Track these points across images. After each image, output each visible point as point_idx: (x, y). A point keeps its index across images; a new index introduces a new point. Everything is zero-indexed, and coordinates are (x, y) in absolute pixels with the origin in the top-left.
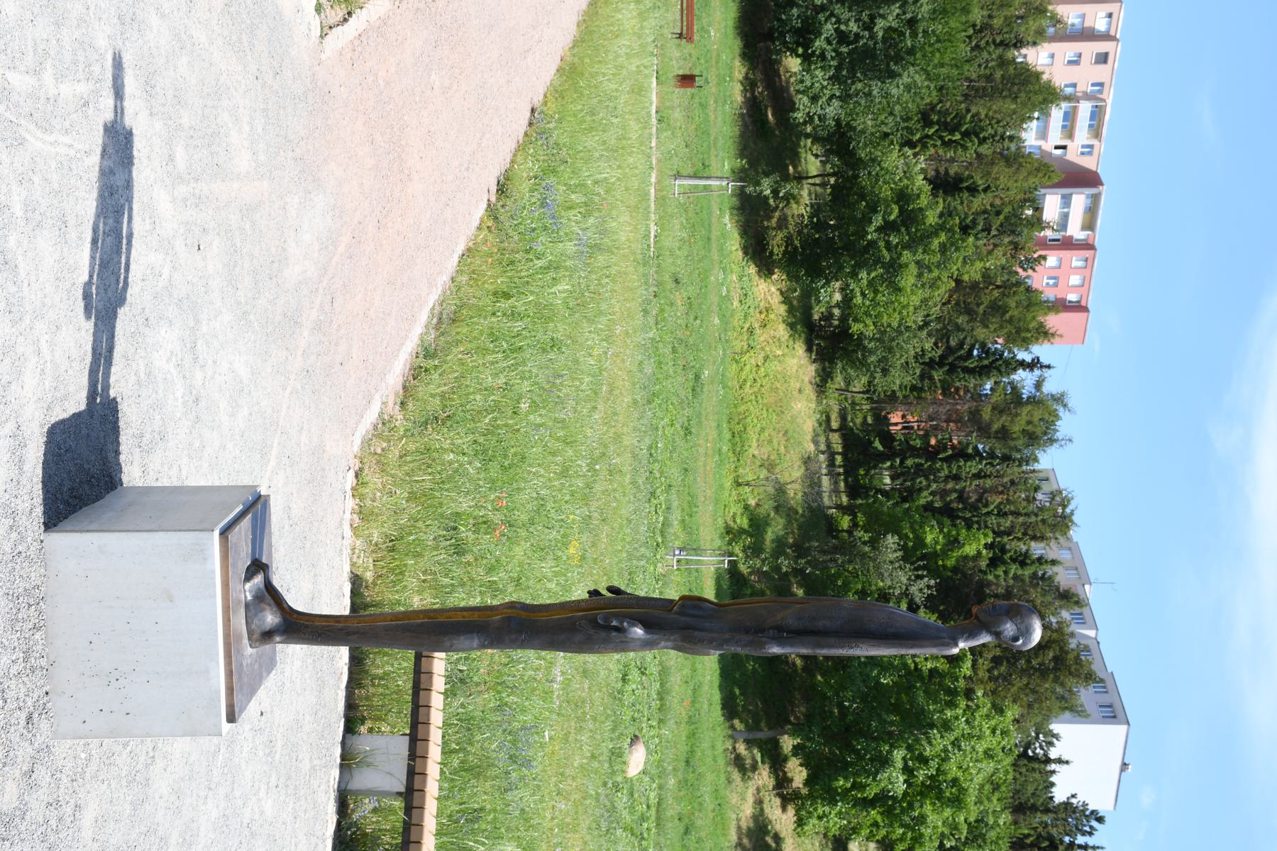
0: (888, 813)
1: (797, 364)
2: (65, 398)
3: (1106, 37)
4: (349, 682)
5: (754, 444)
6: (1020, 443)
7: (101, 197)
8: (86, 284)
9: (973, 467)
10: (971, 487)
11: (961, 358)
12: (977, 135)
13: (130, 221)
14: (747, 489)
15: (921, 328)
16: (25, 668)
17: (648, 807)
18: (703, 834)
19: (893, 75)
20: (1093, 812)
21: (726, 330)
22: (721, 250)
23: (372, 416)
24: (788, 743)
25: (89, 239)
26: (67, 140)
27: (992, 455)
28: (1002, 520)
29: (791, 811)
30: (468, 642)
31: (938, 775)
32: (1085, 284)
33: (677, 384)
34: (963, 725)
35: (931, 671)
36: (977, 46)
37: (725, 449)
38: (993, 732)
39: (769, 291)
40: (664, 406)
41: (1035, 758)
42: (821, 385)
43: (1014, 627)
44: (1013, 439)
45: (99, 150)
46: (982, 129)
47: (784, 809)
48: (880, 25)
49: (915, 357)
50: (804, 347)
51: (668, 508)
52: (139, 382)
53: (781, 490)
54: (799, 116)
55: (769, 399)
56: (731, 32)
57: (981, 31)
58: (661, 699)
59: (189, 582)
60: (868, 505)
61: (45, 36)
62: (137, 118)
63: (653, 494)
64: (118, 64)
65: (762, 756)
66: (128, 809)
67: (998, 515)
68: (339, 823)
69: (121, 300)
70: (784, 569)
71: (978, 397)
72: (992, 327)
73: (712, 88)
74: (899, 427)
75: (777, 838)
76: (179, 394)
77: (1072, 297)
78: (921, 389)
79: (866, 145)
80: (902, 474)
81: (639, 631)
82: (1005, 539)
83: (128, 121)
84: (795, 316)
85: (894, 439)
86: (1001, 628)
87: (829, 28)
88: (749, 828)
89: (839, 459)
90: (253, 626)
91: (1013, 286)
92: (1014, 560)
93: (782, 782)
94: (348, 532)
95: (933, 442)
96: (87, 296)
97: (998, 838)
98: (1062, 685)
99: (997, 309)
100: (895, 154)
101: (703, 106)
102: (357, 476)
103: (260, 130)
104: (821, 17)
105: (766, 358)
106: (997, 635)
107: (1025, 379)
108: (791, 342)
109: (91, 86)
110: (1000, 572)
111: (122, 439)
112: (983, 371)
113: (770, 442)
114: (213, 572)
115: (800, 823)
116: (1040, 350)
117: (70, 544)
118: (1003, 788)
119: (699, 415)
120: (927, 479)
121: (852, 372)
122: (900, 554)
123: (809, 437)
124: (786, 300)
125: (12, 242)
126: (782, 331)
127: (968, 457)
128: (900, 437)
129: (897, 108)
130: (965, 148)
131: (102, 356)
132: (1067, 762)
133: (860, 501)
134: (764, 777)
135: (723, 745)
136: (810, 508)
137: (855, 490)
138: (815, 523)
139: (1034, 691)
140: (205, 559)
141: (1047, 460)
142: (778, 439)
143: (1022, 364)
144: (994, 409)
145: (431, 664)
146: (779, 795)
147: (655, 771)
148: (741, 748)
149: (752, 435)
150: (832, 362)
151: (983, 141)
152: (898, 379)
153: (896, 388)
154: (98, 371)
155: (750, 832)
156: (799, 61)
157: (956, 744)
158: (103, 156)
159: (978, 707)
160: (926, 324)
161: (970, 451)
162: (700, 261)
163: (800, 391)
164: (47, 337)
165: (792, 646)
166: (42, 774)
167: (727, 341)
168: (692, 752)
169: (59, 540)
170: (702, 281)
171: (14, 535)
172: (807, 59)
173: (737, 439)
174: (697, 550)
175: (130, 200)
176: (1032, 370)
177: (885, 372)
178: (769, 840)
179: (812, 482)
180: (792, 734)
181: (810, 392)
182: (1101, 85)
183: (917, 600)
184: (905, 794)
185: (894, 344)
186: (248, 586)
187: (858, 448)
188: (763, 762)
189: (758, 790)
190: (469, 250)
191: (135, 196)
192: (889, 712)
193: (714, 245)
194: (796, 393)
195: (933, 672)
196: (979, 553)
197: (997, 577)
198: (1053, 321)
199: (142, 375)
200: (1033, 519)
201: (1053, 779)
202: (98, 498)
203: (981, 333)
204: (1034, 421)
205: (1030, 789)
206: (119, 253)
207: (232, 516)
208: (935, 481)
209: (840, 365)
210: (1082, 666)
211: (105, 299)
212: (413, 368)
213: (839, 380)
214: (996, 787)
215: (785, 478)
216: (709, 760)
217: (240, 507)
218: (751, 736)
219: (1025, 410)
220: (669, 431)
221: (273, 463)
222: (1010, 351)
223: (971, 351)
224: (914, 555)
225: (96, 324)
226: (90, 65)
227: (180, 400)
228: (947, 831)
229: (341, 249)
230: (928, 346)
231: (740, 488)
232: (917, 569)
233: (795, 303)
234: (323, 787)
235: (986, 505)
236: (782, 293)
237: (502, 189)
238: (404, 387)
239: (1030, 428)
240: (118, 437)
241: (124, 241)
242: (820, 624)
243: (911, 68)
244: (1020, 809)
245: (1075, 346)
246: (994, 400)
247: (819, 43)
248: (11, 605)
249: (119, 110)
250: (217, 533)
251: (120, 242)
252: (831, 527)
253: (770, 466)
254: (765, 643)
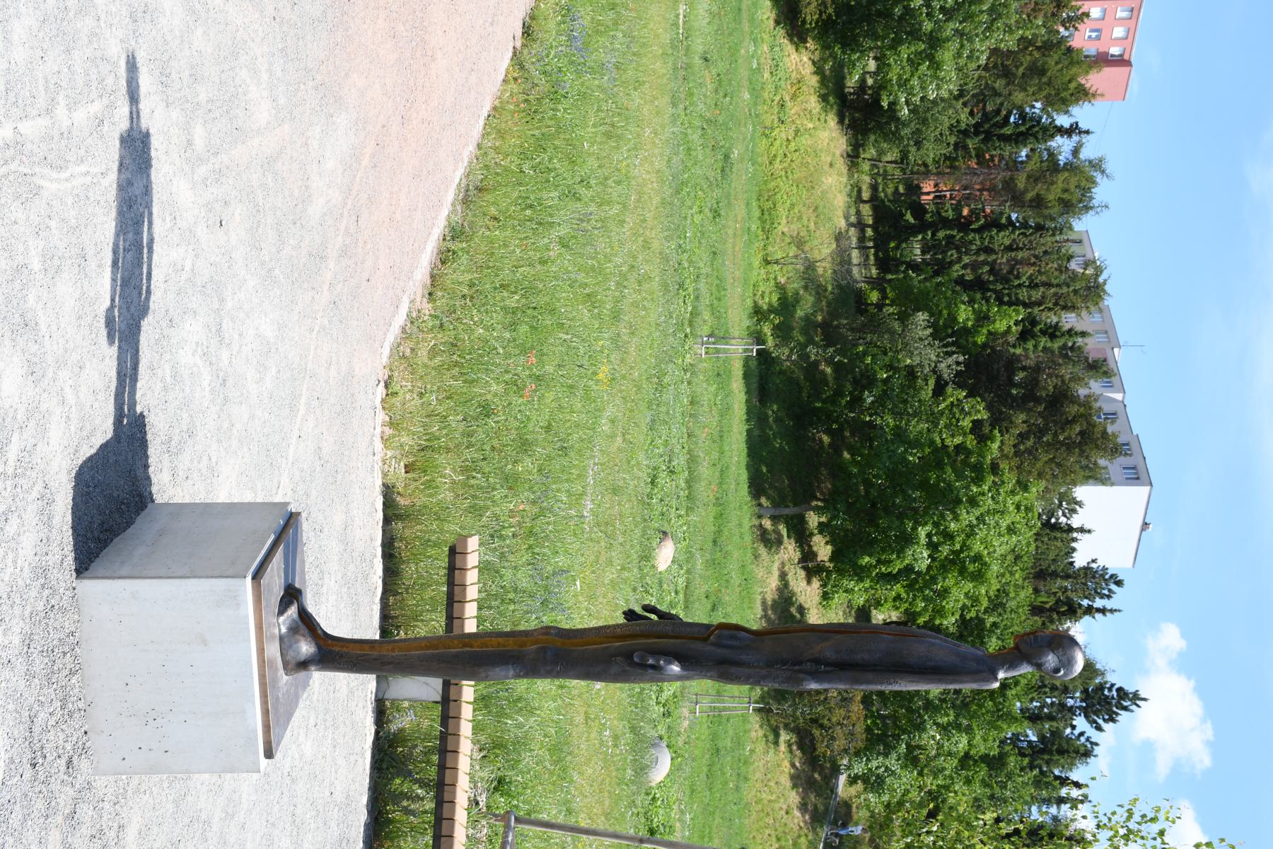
0: (910, 587)
1: (830, 137)
2: (92, 433)
4: (383, 594)
5: (784, 221)
6: (1054, 211)
7: (120, 213)
8: (108, 310)
9: (1004, 238)
10: (1003, 259)
11: (997, 125)
13: (150, 223)
14: (776, 267)
15: (957, 98)
16: (63, 715)
17: (676, 592)
18: (729, 609)
20: (1112, 576)
21: (756, 104)
22: (752, 20)
23: (400, 319)
24: (813, 520)
25: (109, 263)
26: (83, 168)
27: (1025, 225)
28: (1033, 293)
29: (816, 583)
30: (503, 673)
31: (961, 551)
32: (1130, 36)
33: (706, 165)
34: (990, 501)
35: (957, 447)
37: (754, 227)
38: (1018, 507)
39: (799, 62)
41: (1057, 527)
42: (853, 158)
43: (1056, 659)
44: (1047, 208)
45: (115, 166)
47: (809, 582)
50: (836, 119)
51: (697, 298)
52: (165, 389)
53: (810, 266)
58: (689, 487)
59: (222, 621)
60: (898, 279)
61: (56, 69)
62: (154, 118)
63: (681, 285)
64: (132, 66)
65: (788, 531)
66: (170, 807)
67: (1029, 286)
68: (377, 733)
69: (144, 311)
70: (813, 357)
71: (1015, 165)
72: (1031, 90)
74: (931, 197)
75: (801, 609)
76: (205, 383)
77: (1115, 51)
78: (956, 159)
80: (934, 246)
81: (675, 668)
82: (1036, 310)
83: (144, 123)
84: (827, 87)
85: (926, 211)
86: (1043, 660)
88: (774, 600)
89: (869, 232)
90: (288, 658)
91: (1052, 45)
92: (1043, 332)
93: (808, 556)
94: (378, 445)
95: (965, 212)
96: (109, 322)
97: (1018, 607)
98: (1087, 457)
99: (1037, 70)
102: (386, 387)
103: (279, 74)
105: (797, 132)
106: (1039, 666)
107: (1062, 146)
109: (105, 101)
110: (1030, 345)
111: (151, 451)
112: (1019, 138)
113: (800, 218)
114: (247, 617)
115: (825, 596)
116: (1081, 114)
117: (104, 594)
118: (1025, 558)
120: (959, 252)
122: (929, 331)
123: (840, 213)
124: (819, 71)
125: (31, 299)
126: (814, 103)
127: (1001, 227)
128: (931, 208)
131: (127, 375)
132: (1089, 531)
133: (889, 277)
134: (790, 550)
135: (748, 522)
136: (839, 287)
137: (885, 264)
138: (847, 299)
139: (1059, 465)
140: (238, 605)
141: (1081, 224)
142: (808, 214)
143: (1061, 131)
144: (1029, 177)
145: (464, 577)
146: (804, 568)
147: (683, 561)
148: (767, 524)
149: (782, 212)
152: (931, 151)
154: (123, 393)
155: (775, 604)
157: (980, 519)
158: (120, 170)
159: (1003, 482)
161: (1004, 221)
162: (730, 34)
163: (831, 165)
164: (70, 382)
165: (829, 681)
166: (85, 812)
167: (757, 116)
168: (719, 532)
169: (90, 587)
170: (732, 55)
171: (47, 592)
173: (766, 217)
174: (725, 338)
175: (149, 206)
176: (1070, 136)
177: (918, 144)
178: (793, 610)
179: (842, 259)
180: (818, 510)
181: (841, 165)
183: (946, 376)
184: (929, 567)
185: (929, 115)
186: (282, 619)
187: (889, 220)
188: (789, 537)
189: (783, 564)
190: (495, 108)
191: (154, 199)
192: (915, 489)
193: (745, 15)
194: (826, 168)
195: (958, 448)
196: (1010, 327)
197: (1026, 350)
198: (1093, 80)
199: (168, 379)
200: (1065, 290)
201: (1074, 545)
202: (129, 524)
204: (1072, 187)
205: (1052, 556)
206: (140, 265)
207: (263, 552)
208: (966, 253)
209: (872, 138)
210: (1109, 440)
211: (126, 322)
212: (440, 252)
213: (871, 152)
214: (1018, 558)
215: (816, 255)
216: (736, 539)
217: (272, 537)
218: (777, 513)
219: (1061, 177)
220: (698, 218)
221: (302, 412)
222: (1049, 115)
223: (1007, 118)
224: (945, 332)
225: (119, 348)
226: (103, 80)
227: (208, 389)
228: (968, 603)
229: (365, 162)
231: (769, 267)
232: (945, 346)
233: (828, 73)
234: (360, 705)
235: (1018, 277)
236: (814, 63)
237: (527, 31)
238: (432, 276)
239: (1065, 196)
240: (146, 451)
241: (145, 250)
242: (858, 657)
244: (1041, 575)
245: (1116, 103)
246: (1029, 168)
248: (46, 660)
249: (135, 116)
250: (249, 578)
251: (141, 253)
252: (859, 297)
253: (799, 243)
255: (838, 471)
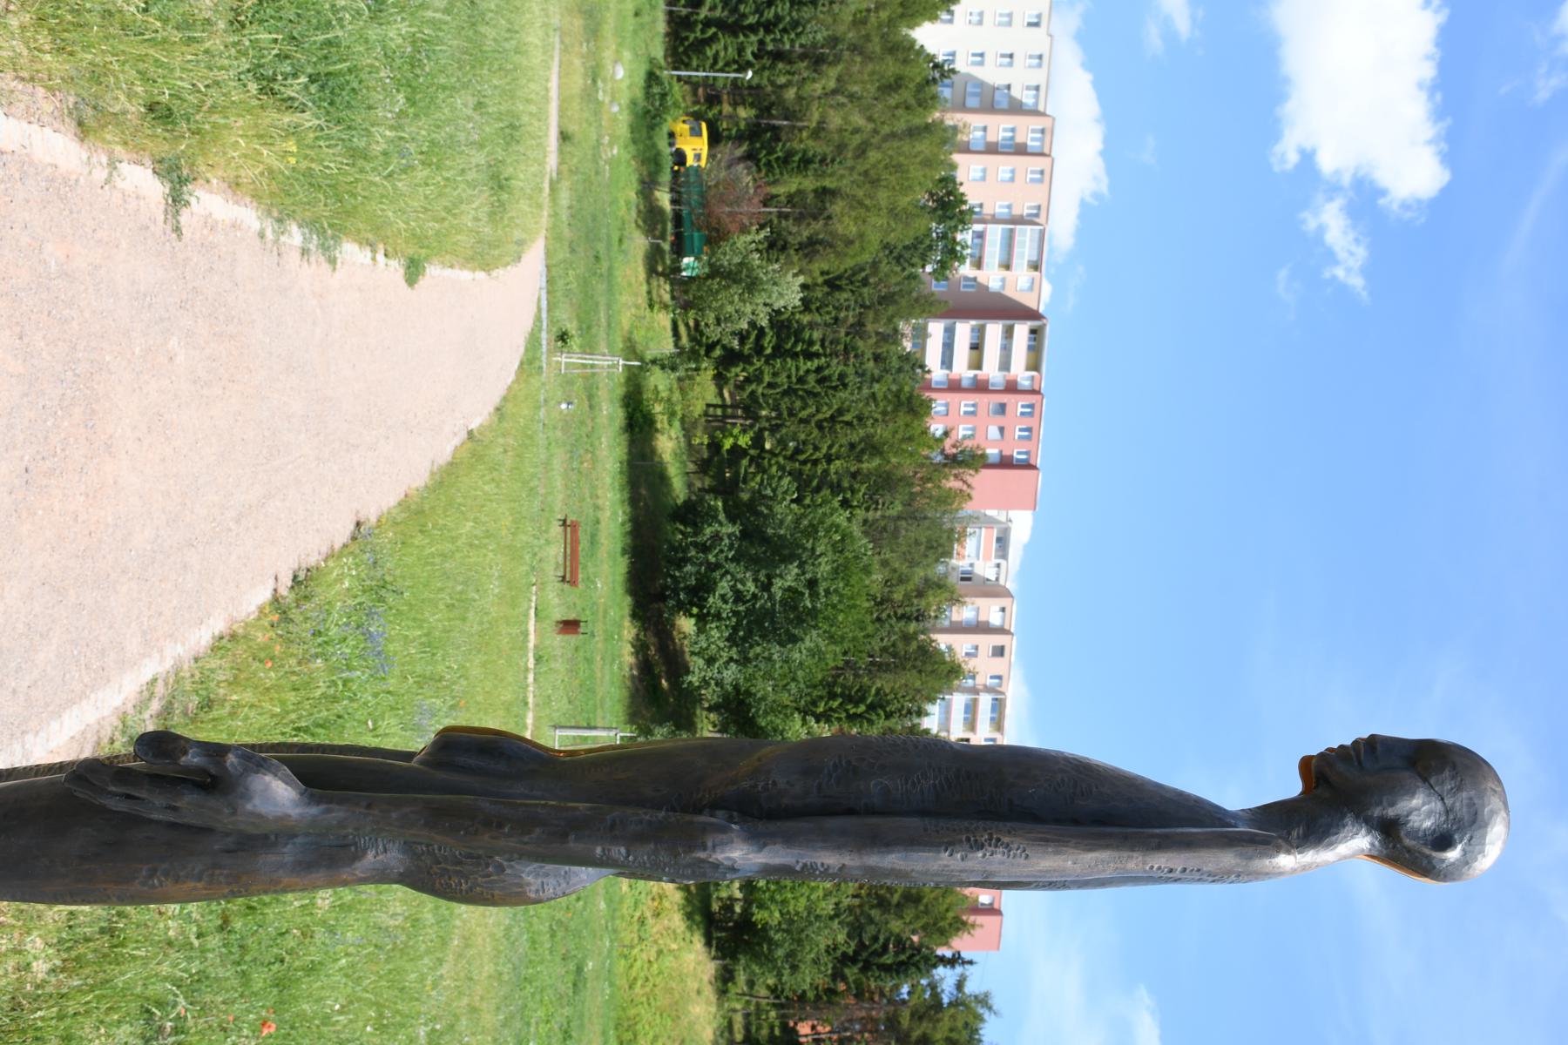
1: (695, 961)
3: (1001, 630)
12: (883, 707)
15: (832, 918)
19: (794, 639)
21: (613, 918)
33: (553, 974)
36: (879, 619)
40: (538, 997)
42: (725, 979)
46: (888, 703)
48: (778, 583)
49: (827, 951)
54: (694, 679)
55: (662, 1001)
56: (620, 589)
57: (881, 603)
73: (598, 643)
79: (766, 713)
87: (724, 586)
100: (798, 722)
101: (589, 661)
104: (717, 574)
105: (660, 952)
108: (688, 935)
119: (581, 1017)
121: (755, 968)
126: (677, 921)
129: (800, 673)
130: (871, 722)
143: (943, 960)
144: (912, 1015)
150: (734, 958)
151: (888, 716)
153: (806, 987)
156: (693, 621)
160: (837, 915)
163: (699, 992)
172: (702, 619)
176: (953, 967)
181: (709, 993)
182: (999, 677)
194: (693, 994)
203: (896, 925)
209: (743, 962)
220: (543, 1029)
230: (841, 938)
243: (814, 633)
247: (713, 601)
254: (705, 829)
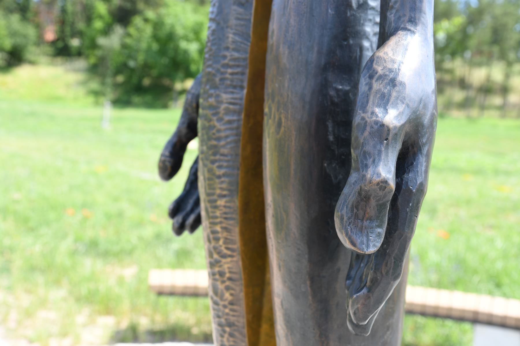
1: (23, 72)
42: (32, 63)
138: (95, 70)
152: (31, 31)
179: (76, 71)
187: (62, 51)
224: (107, 31)
255: (160, 76)
